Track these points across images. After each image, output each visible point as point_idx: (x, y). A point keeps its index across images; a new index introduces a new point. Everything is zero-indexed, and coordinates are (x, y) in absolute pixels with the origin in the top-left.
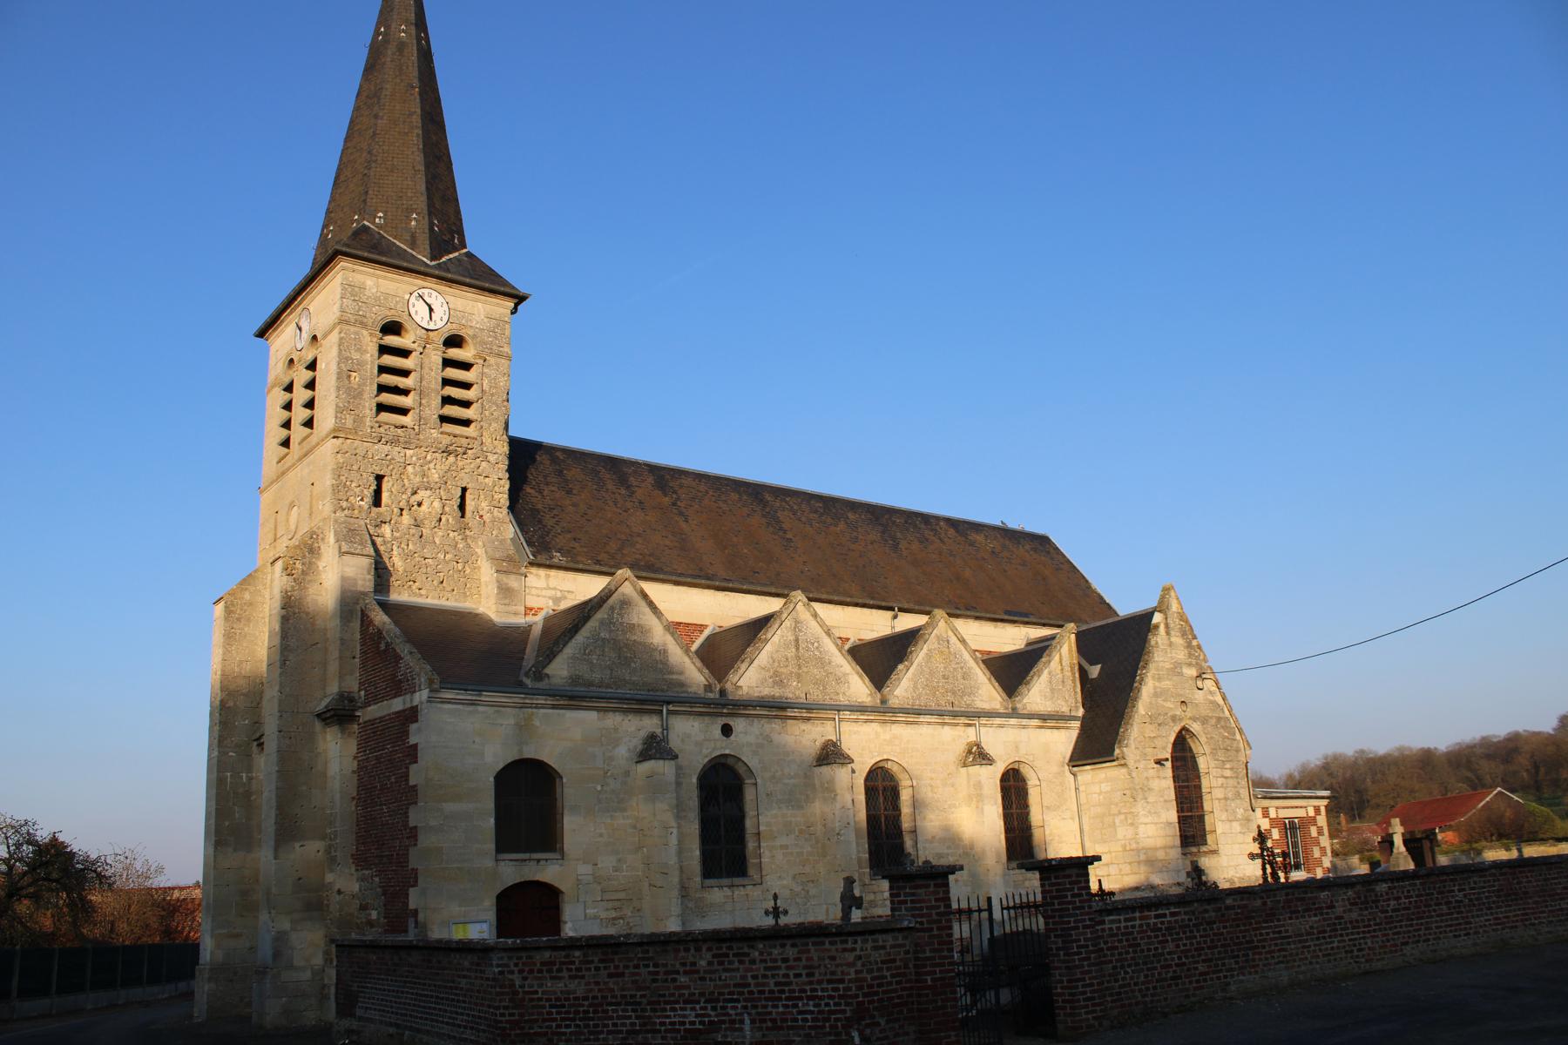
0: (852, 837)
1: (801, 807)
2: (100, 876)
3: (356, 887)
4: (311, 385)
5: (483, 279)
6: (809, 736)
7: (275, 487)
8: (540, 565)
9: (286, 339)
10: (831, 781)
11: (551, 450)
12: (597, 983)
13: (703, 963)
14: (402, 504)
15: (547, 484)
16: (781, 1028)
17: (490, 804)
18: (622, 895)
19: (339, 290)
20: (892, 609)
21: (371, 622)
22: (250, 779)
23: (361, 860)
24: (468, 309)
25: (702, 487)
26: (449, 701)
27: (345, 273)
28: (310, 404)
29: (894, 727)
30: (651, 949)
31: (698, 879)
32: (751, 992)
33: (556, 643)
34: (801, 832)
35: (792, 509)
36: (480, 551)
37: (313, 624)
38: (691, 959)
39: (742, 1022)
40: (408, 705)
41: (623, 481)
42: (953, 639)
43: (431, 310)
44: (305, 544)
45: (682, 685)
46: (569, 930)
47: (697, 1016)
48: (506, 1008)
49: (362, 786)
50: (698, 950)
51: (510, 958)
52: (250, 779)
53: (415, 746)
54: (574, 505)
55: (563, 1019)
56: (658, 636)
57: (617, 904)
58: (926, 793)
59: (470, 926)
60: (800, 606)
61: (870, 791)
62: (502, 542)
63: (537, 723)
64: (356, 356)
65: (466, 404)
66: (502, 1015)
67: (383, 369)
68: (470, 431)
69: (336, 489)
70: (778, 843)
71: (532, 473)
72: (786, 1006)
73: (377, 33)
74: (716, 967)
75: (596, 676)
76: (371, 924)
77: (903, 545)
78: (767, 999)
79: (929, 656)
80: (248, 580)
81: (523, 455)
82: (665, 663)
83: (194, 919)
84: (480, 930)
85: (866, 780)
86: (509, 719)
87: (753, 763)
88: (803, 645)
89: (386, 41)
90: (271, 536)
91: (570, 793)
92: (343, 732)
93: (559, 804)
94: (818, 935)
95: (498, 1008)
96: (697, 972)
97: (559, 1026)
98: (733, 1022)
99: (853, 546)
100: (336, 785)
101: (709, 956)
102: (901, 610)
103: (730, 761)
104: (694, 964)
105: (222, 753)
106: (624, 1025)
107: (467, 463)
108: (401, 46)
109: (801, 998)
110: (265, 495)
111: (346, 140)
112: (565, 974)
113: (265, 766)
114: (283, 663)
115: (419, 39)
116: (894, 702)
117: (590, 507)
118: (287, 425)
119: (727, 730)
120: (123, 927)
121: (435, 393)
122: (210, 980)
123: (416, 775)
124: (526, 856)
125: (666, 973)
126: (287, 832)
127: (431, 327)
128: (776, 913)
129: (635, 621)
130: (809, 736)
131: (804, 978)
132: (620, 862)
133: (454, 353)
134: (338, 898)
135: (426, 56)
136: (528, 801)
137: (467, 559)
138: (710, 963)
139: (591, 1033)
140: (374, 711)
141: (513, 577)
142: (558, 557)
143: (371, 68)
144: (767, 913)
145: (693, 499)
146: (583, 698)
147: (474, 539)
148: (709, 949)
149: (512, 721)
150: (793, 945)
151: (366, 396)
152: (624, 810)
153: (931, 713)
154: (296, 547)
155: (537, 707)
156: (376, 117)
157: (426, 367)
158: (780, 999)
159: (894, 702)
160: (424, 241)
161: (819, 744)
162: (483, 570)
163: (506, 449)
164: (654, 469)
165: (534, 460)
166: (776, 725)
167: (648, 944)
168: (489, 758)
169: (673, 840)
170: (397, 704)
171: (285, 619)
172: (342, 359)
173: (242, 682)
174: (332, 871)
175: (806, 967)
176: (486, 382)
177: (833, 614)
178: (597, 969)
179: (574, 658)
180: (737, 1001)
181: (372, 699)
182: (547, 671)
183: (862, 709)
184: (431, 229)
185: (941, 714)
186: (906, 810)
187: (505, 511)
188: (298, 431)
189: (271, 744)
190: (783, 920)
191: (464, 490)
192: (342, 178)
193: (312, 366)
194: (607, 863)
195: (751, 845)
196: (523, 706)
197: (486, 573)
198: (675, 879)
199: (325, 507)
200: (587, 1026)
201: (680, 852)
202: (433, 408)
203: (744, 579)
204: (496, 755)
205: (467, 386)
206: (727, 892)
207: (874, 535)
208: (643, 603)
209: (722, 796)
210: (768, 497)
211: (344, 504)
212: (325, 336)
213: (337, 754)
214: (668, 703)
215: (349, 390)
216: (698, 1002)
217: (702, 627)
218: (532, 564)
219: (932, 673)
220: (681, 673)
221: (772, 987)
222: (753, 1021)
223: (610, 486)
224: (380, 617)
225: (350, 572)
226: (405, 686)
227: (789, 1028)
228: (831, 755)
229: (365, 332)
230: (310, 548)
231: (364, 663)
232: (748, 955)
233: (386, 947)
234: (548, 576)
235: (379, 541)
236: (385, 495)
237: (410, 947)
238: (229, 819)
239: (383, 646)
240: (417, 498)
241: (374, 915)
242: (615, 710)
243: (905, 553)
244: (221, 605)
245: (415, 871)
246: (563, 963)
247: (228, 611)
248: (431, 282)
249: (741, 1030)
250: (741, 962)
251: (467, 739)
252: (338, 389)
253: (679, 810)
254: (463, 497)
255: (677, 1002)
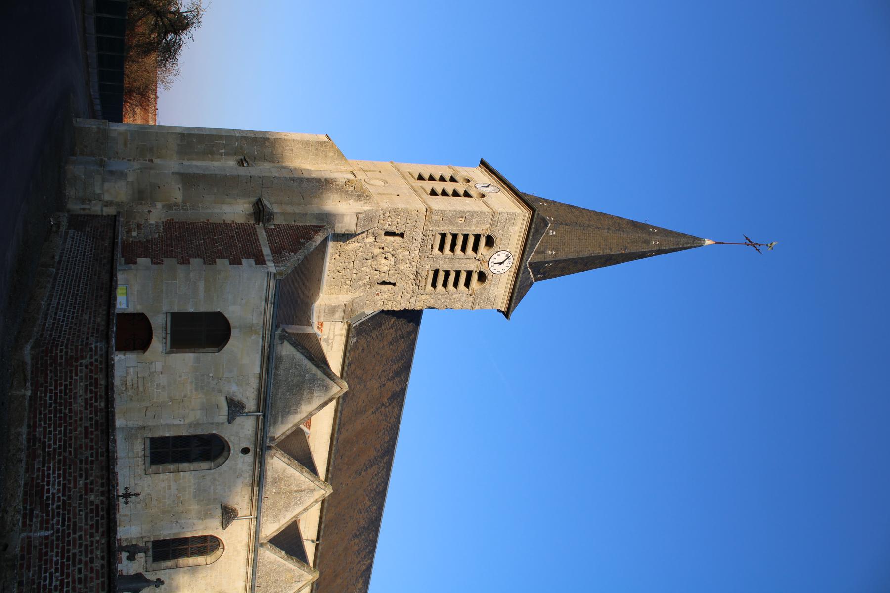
0: (174, 531)
1: (195, 497)
2: (166, 60)
3: (152, 222)
4: (456, 194)
5: (517, 294)
6: (241, 501)
7: (395, 171)
8: (348, 330)
9: (481, 177)
10: (211, 516)
11: (415, 331)
12: (81, 419)
13: (93, 498)
14: (386, 249)
15: (396, 331)
16: (40, 560)
17: (202, 309)
18: (141, 389)
19: (512, 211)
20: (318, 539)
21: (317, 233)
22: (221, 154)
23: (169, 225)
24: (501, 285)
25: (392, 420)
26: (268, 284)
27: (522, 214)
28: (444, 193)
29: (245, 552)
30: (104, 458)
31: (150, 436)
32: (69, 535)
33: (303, 348)
34: (179, 498)
35: (378, 473)
36: (357, 294)
37: (315, 197)
38: (96, 488)
39: (47, 529)
40: (266, 258)
41: (397, 374)
42: (300, 584)
43: (501, 264)
44: (363, 193)
45: (275, 423)
46: (119, 358)
47: (54, 494)
48: (67, 353)
49: (216, 226)
50: (102, 493)
51: (101, 356)
52: (221, 154)
53: (241, 264)
54: (383, 347)
55: (56, 394)
56: (305, 409)
57: (136, 386)
58: (201, 574)
59: (125, 297)
60: (323, 492)
61: (205, 538)
62: (363, 307)
63: (253, 337)
64: (474, 221)
65: (445, 284)
66: (61, 351)
67: (466, 237)
68: (429, 287)
69: (396, 210)
70: (172, 483)
71: (402, 321)
72: (57, 564)
73: (654, 228)
74: (89, 507)
75: (281, 372)
76: (129, 231)
77: (357, 541)
78: (63, 547)
79: (290, 570)
80: (340, 155)
81: (413, 317)
82: (289, 413)
83: (137, 105)
84: (123, 303)
85: (211, 536)
86: (256, 320)
87: (224, 467)
88: (298, 494)
89: (649, 233)
90: (366, 168)
91: (208, 357)
92: (250, 215)
93: (201, 350)
94: (109, 585)
95: (66, 347)
96: (86, 494)
97: (51, 391)
98: (48, 522)
99: (356, 511)
100: (217, 211)
101: (97, 502)
102: (317, 545)
103: (226, 453)
104: (92, 490)
105: (237, 139)
106: (50, 439)
107: (410, 285)
108: (647, 242)
109: (62, 575)
110: (390, 164)
111: (594, 211)
112: (89, 396)
113: (228, 164)
114: (293, 180)
115: (651, 251)
116: (261, 551)
117: (382, 356)
118: (431, 178)
119: (245, 451)
120: (135, 67)
121: (452, 267)
122: (99, 128)
123: (222, 263)
124: (169, 331)
125: (86, 469)
126: (189, 180)
127: (491, 264)
128: (126, 495)
129: (316, 394)
130: (241, 501)
131: (77, 576)
132: (162, 387)
133: (475, 277)
134: (146, 211)
135: (642, 255)
136: (204, 332)
137: (352, 285)
138: (92, 503)
139: (45, 415)
140: (262, 235)
141: (342, 314)
142: (353, 340)
143: (635, 225)
144: (126, 488)
145: (386, 416)
146: (268, 365)
147: (364, 291)
148: (102, 502)
149: (254, 322)
150: (103, 566)
151: (451, 227)
152: (196, 390)
153: (254, 574)
154: (362, 187)
155: (263, 338)
156: (608, 229)
157: (467, 261)
158: (63, 558)
159: (261, 551)
160: (540, 258)
161: (236, 506)
162: (345, 296)
163: (418, 308)
164: (403, 391)
165: (409, 322)
166: (248, 480)
167: (108, 456)
168: (232, 308)
169: (176, 422)
170: (266, 251)
171: (318, 180)
172: (472, 213)
173: (280, 151)
174: (163, 207)
175: (86, 576)
176: (458, 296)
177: (314, 514)
178: (91, 419)
179: (293, 358)
180: (63, 525)
181: (270, 234)
182: (286, 343)
183: (257, 532)
184: (546, 262)
185: (253, 580)
186: (191, 561)
187: (381, 308)
188: (428, 185)
189: (243, 171)
190: (121, 500)
191: (394, 284)
192: (573, 210)
193: (467, 194)
194: (163, 380)
195: (171, 467)
196: (264, 329)
197: (344, 298)
198: (150, 423)
199: (385, 204)
200: (50, 412)
201: (168, 425)
202: (443, 266)
203: (338, 451)
204: (233, 313)
205: (456, 284)
206: (141, 454)
207: (363, 523)
208: (326, 399)
209: (206, 448)
210: (386, 458)
211: (387, 215)
212: (485, 202)
213: (236, 211)
214: (264, 416)
215: (454, 217)
216: (64, 495)
217: (309, 427)
218: (349, 325)
219: (279, 573)
220: (282, 423)
221: (73, 551)
222: (47, 537)
223: (394, 367)
224: (319, 238)
225: (347, 220)
226: (278, 256)
227: (40, 567)
228: (228, 515)
229: (487, 226)
230: (361, 195)
231: (290, 228)
232: (97, 531)
233: (113, 254)
234: (341, 335)
235: (365, 235)
236: (391, 238)
237: (112, 262)
238: (197, 142)
239: (302, 241)
240: (390, 257)
241: (134, 234)
242: (260, 384)
243: (352, 542)
244: (326, 140)
245: (161, 263)
246: (96, 393)
247: (322, 144)
248: (516, 263)
249: (41, 529)
250: (92, 526)
251: (243, 295)
252: (455, 211)
253: (197, 424)
254: (390, 283)
255: (64, 479)
